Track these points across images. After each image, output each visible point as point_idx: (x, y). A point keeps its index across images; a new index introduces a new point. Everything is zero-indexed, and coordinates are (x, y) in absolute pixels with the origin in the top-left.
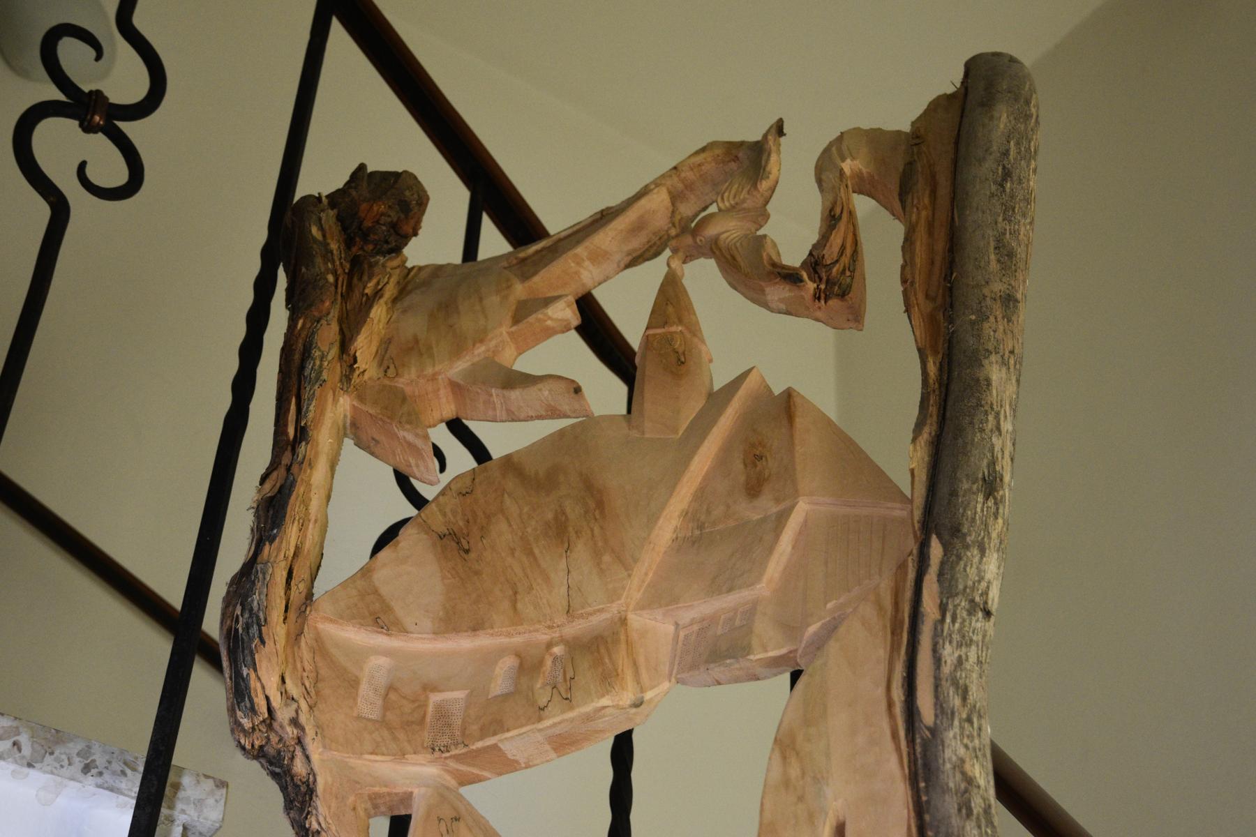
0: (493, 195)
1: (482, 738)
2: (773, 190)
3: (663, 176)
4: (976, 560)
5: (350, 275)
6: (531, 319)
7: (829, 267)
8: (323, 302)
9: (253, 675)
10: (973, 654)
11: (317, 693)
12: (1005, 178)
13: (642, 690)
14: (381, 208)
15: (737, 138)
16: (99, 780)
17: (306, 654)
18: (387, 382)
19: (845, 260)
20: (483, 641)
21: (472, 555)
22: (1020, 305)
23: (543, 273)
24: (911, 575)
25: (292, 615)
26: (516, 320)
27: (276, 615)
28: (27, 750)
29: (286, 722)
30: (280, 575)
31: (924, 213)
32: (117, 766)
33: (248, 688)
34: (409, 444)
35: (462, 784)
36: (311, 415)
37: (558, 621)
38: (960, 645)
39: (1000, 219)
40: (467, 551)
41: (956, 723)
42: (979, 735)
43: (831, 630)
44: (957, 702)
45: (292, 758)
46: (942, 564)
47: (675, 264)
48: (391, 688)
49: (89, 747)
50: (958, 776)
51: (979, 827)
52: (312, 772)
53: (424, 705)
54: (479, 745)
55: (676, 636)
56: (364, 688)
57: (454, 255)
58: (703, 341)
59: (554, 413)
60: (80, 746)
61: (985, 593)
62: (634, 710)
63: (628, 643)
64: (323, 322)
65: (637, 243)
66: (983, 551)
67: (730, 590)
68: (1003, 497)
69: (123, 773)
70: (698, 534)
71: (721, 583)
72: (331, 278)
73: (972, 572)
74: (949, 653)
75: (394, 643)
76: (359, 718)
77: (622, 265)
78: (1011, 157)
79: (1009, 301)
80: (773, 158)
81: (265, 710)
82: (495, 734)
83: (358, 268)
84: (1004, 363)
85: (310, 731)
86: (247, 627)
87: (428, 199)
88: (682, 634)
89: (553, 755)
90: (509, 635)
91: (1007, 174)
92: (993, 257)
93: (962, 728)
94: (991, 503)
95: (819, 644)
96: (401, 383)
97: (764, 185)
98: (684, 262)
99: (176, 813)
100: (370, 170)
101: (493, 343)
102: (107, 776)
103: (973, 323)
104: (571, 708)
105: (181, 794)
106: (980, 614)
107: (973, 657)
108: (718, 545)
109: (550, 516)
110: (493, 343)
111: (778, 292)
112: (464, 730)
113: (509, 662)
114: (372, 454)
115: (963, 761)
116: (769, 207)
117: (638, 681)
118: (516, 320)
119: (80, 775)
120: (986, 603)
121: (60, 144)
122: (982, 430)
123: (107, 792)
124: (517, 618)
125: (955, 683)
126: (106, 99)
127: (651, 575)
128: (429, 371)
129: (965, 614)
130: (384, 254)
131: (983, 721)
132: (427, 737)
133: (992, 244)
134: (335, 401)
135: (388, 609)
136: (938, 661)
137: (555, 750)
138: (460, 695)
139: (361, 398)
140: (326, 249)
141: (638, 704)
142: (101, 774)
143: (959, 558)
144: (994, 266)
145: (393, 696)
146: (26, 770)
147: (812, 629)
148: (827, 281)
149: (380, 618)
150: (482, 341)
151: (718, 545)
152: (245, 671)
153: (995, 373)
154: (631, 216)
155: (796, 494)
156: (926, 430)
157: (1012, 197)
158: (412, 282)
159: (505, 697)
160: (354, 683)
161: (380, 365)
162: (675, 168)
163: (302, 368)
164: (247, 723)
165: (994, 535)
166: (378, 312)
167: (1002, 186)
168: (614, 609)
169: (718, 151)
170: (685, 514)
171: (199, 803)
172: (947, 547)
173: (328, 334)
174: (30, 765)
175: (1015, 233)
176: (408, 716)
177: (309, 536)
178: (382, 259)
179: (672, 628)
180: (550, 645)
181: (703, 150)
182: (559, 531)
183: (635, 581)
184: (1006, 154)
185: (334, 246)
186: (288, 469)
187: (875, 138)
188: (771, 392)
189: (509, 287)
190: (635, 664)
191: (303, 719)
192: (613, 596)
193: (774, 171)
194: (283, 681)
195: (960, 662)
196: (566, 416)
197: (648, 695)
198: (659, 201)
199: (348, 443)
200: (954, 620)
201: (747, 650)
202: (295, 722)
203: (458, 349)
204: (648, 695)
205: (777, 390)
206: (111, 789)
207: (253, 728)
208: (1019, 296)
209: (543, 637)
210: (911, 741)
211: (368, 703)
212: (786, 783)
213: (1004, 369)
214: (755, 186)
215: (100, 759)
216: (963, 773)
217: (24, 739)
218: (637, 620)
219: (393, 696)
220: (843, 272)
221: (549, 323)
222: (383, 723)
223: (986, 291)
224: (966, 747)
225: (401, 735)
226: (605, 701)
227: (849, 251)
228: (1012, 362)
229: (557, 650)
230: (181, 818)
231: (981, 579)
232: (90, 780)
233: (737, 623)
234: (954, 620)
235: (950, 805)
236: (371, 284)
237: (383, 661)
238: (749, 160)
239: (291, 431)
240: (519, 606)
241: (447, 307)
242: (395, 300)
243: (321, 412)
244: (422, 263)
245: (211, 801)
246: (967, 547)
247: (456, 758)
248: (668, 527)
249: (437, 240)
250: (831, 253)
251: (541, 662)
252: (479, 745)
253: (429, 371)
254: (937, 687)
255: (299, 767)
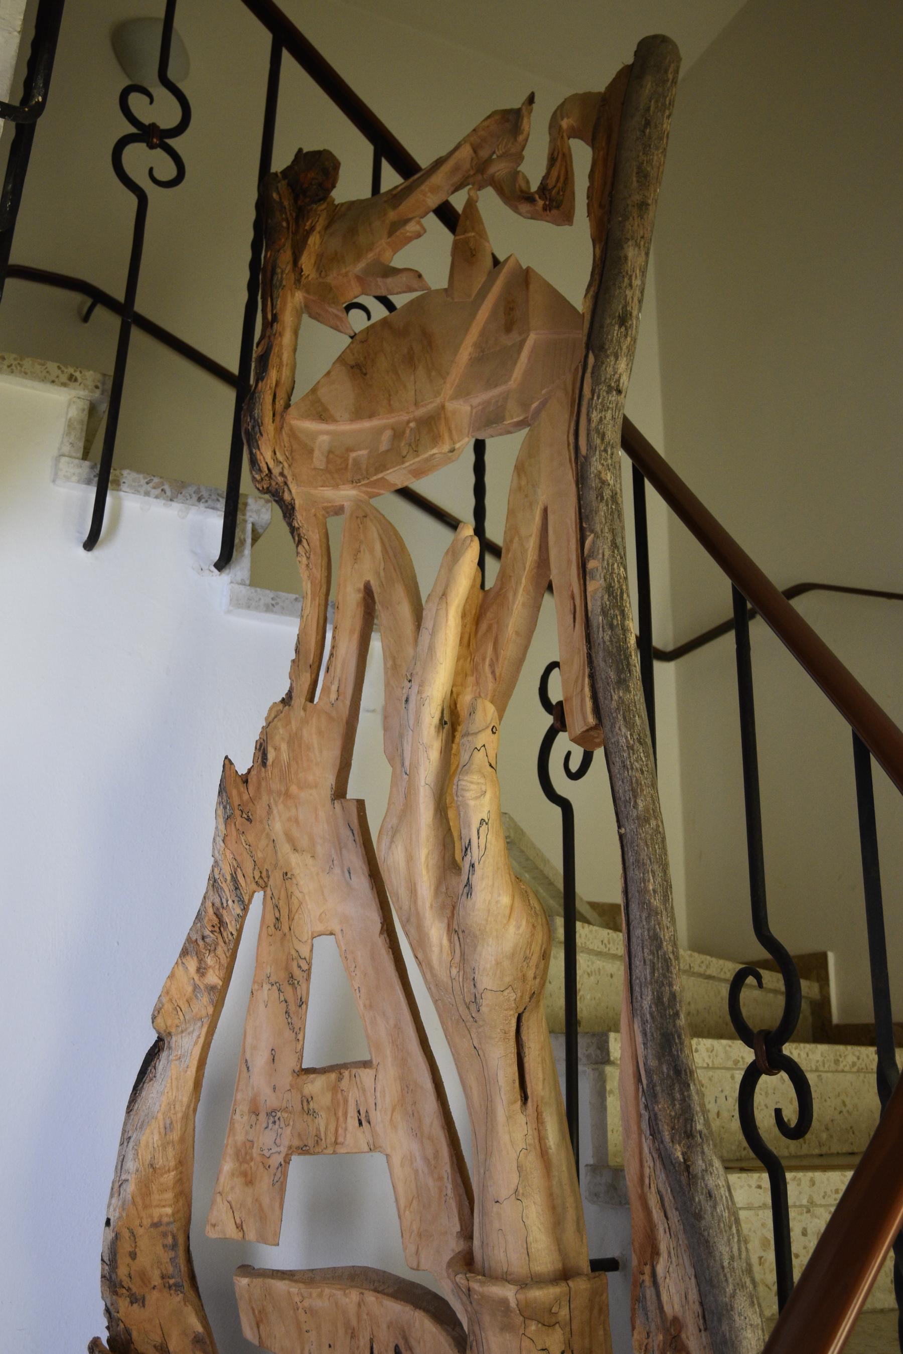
0: (387, 148)
1: (375, 475)
2: (526, 140)
3: (468, 135)
4: (613, 363)
5: (297, 220)
6: (398, 233)
7: (550, 191)
8: (280, 239)
9: (258, 453)
10: (609, 415)
11: (292, 458)
12: (645, 127)
13: (454, 443)
14: (317, 169)
15: (508, 107)
16: (206, 505)
17: (286, 439)
18: (321, 280)
19: (560, 185)
20: (375, 422)
21: (368, 376)
22: (650, 207)
23: (404, 204)
24: (580, 374)
25: (278, 418)
26: (390, 234)
27: (268, 419)
28: (169, 493)
29: (277, 475)
30: (268, 399)
31: (601, 153)
32: (214, 497)
33: (256, 459)
34: (336, 316)
35: (370, 497)
36: (278, 307)
37: (411, 410)
38: (601, 411)
39: (641, 154)
40: (365, 374)
41: (597, 453)
42: (611, 458)
43: (543, 404)
44: (598, 441)
45: (283, 492)
46: (594, 367)
47: (472, 193)
48: (330, 452)
49: (199, 489)
50: (597, 480)
51: (607, 505)
52: (293, 499)
53: (347, 460)
54: (375, 478)
55: (471, 413)
56: (317, 453)
57: (365, 192)
58: (488, 242)
59: (410, 290)
60: (194, 489)
61: (618, 380)
62: (450, 454)
63: (446, 419)
64: (282, 251)
65: (457, 179)
66: (617, 358)
67: (496, 386)
68: (631, 325)
69: (218, 500)
70: (481, 357)
71: (490, 384)
72: (284, 224)
73: (610, 370)
74: (595, 416)
75: (331, 427)
76: (315, 469)
77: (452, 189)
78: (651, 112)
79: (643, 206)
80: (525, 120)
81: (266, 470)
82: (382, 472)
83: (301, 214)
84: (637, 245)
85: (290, 478)
86: (253, 427)
87: (339, 164)
88: (474, 411)
89: (414, 480)
90: (387, 418)
91: (648, 123)
92: (634, 179)
93: (600, 455)
94: (623, 329)
95: (538, 411)
96: (329, 280)
97: (521, 138)
98: (479, 190)
99: (247, 517)
100: (305, 151)
101: (378, 250)
102: (210, 502)
103: (620, 222)
104: (418, 456)
105: (248, 508)
106: (614, 393)
107: (609, 415)
108: (492, 360)
109: (406, 351)
110: (378, 250)
111: (525, 207)
112: (367, 470)
113: (388, 434)
114: (319, 321)
115: (600, 472)
116: (524, 153)
117: (451, 438)
118: (390, 234)
119: (197, 503)
120: (618, 386)
121: (138, 159)
122: (620, 288)
123: (211, 511)
124: (391, 410)
125: (598, 431)
126: (158, 127)
127: (457, 380)
128: (344, 271)
129: (605, 394)
130: (315, 202)
131: (615, 450)
132: (349, 475)
133: (635, 170)
134: (293, 296)
135: (325, 409)
136: (589, 420)
137: (415, 477)
138: (364, 452)
139: (307, 291)
140: (292, 198)
141: (452, 451)
142: (206, 501)
143: (603, 363)
144: (635, 184)
145: (331, 456)
146: (170, 503)
147: (534, 405)
148: (551, 201)
149: (322, 415)
150: (371, 250)
151: (492, 360)
152: (254, 451)
153: (631, 252)
154: (451, 163)
155: (528, 331)
156: (592, 289)
157: (650, 138)
158: (338, 214)
159: (387, 451)
160: (311, 451)
161: (317, 270)
162: (474, 130)
163: (272, 279)
164: (258, 477)
165: (624, 347)
166: (314, 241)
167: (644, 132)
168: (438, 400)
169: (497, 117)
170: (475, 345)
171: (258, 512)
172: (596, 358)
173: (286, 257)
174: (171, 500)
175: (650, 162)
176: (339, 467)
177: (284, 374)
178: (315, 206)
179: (469, 408)
180: (408, 422)
181: (489, 117)
182: (410, 360)
183: (448, 385)
184: (648, 109)
185: (286, 203)
186: (269, 337)
187: (584, 99)
188: (521, 267)
189: (385, 215)
190: (450, 430)
191: (286, 472)
192: (437, 394)
193: (527, 129)
194: (275, 454)
195: (601, 419)
196: (416, 290)
197: (457, 446)
198: (466, 152)
199: (305, 317)
200: (598, 398)
201: (503, 419)
202: (282, 474)
203: (358, 257)
204: (457, 446)
205: (524, 267)
206: (213, 508)
207: (262, 479)
208: (650, 202)
209: (405, 417)
210: (577, 463)
211: (319, 460)
212: (520, 488)
213: (637, 249)
214: (516, 140)
215: (205, 493)
216: (600, 479)
217: (166, 487)
218: (450, 406)
219: (331, 456)
220: (558, 193)
221: (408, 234)
222: (327, 470)
223: (629, 202)
224: (603, 465)
225: (336, 476)
226: (435, 451)
227: (562, 180)
228: (642, 243)
229: (412, 425)
230: (250, 520)
231: (616, 373)
232: (202, 506)
233: (499, 404)
234: (598, 398)
235: (592, 495)
236: (308, 224)
237: (325, 438)
238: (511, 121)
239: (270, 317)
240: (392, 402)
241: (352, 231)
242: (327, 227)
243: (284, 303)
244: (343, 201)
245: (264, 510)
246: (607, 357)
247: (365, 485)
248: (465, 353)
249: (352, 185)
250: (551, 182)
251: (404, 432)
252: (375, 478)
253: (344, 271)
254: (588, 434)
255: (287, 497)
